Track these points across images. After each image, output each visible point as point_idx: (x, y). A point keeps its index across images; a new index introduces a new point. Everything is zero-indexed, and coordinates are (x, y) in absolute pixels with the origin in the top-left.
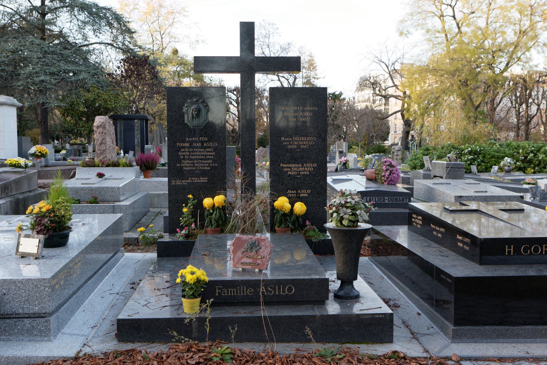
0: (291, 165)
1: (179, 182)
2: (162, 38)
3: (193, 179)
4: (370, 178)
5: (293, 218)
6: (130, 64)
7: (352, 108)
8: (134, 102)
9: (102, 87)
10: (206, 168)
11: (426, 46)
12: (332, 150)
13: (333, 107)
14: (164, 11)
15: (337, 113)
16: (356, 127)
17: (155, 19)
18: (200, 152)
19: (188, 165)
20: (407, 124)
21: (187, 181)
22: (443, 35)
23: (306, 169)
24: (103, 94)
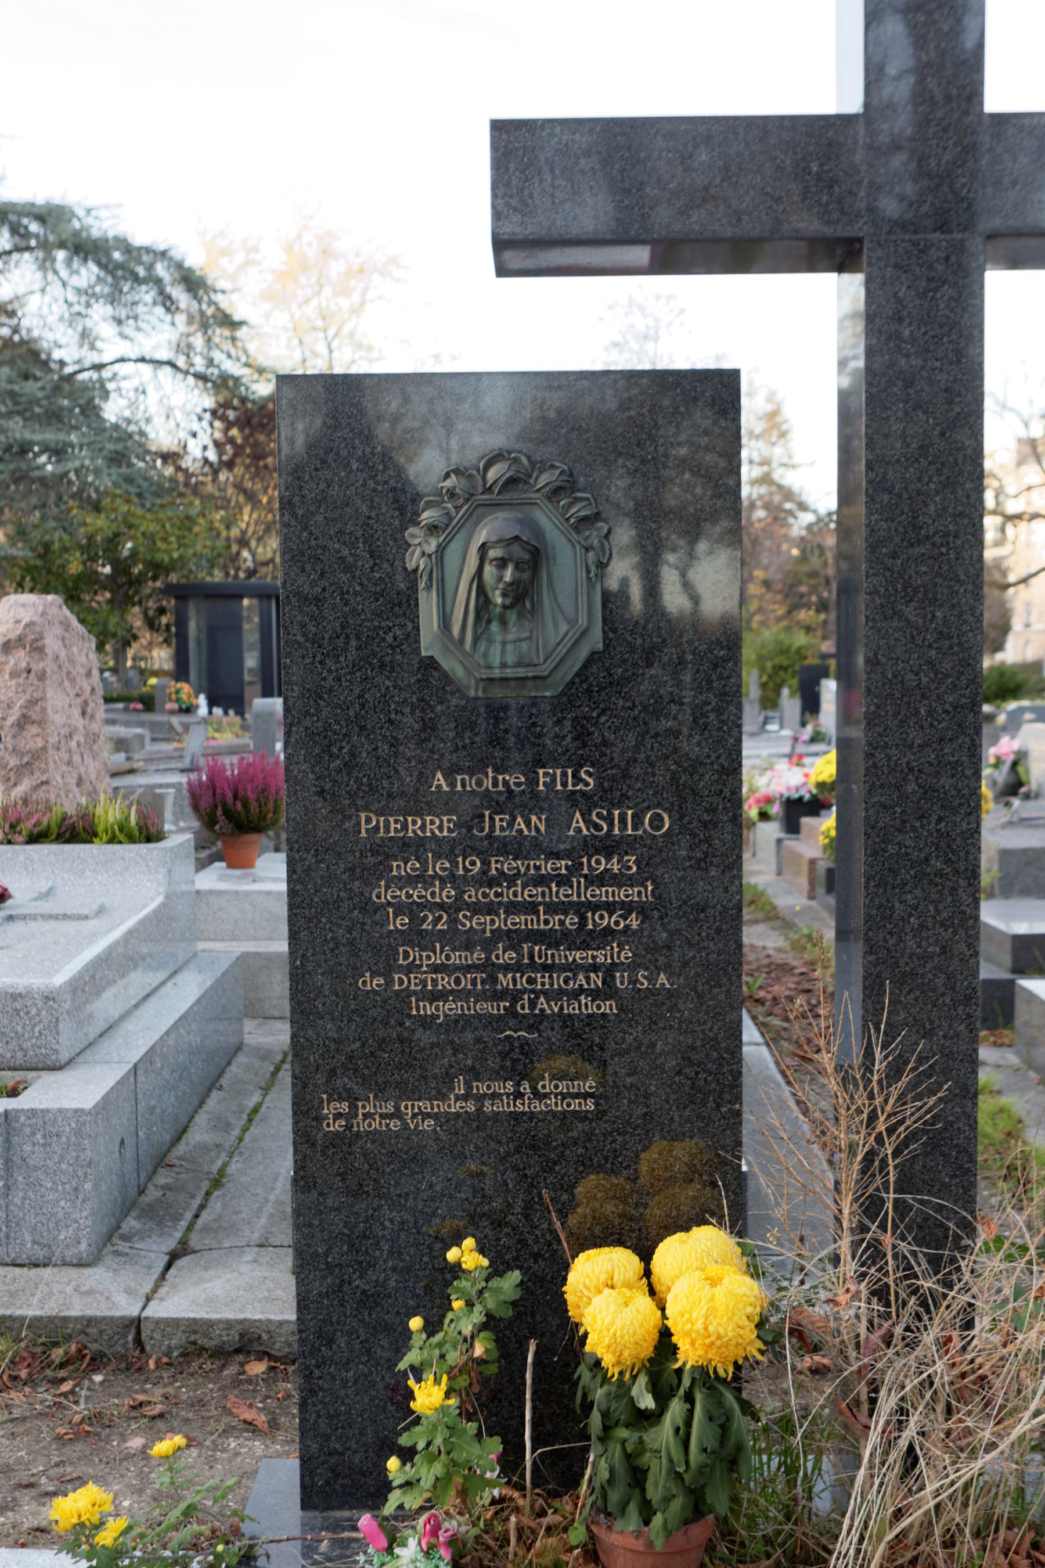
1: (374, 1115)
3: (481, 1088)
6: (229, 425)
8: (243, 542)
9: (140, 495)
10: (587, 1006)
14: (336, 268)
17: (309, 292)
18: (541, 880)
19: (445, 982)
21: (439, 1107)
24: (143, 518)
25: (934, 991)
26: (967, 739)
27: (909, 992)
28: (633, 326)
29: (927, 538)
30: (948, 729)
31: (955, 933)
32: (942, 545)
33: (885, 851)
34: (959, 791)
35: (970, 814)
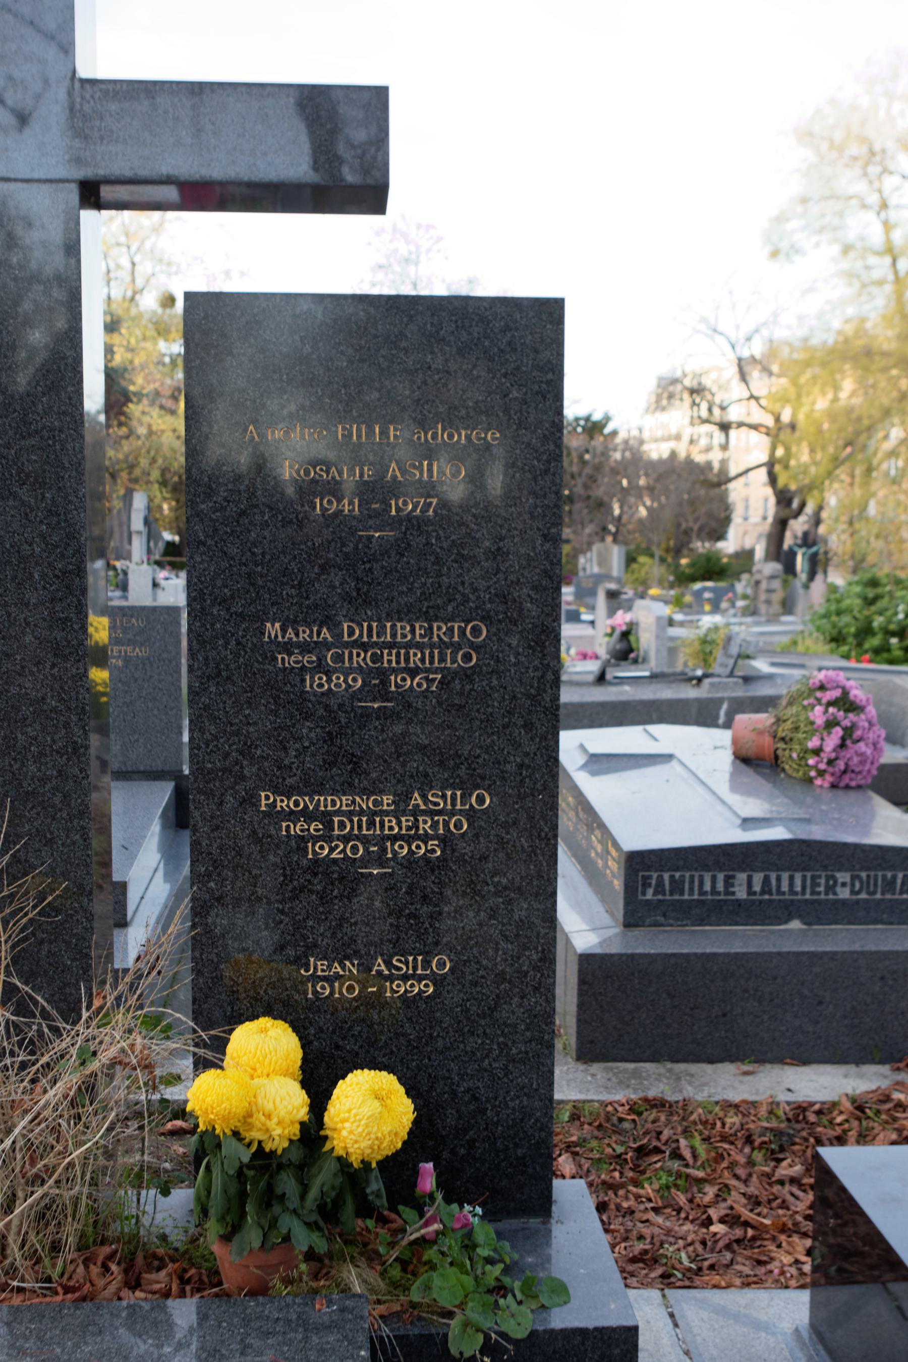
0: (325, 802)
2: (133, 264)
4: (751, 752)
5: (323, 1178)
7: (635, 460)
11: (840, 290)
12: (584, 569)
13: (587, 451)
15: (598, 468)
16: (644, 505)
20: (787, 503)
22: (888, 260)
23: (425, 825)
25: (52, 807)
26: (75, 599)
27: (32, 809)
28: (396, 251)
29: (36, 432)
30: (58, 590)
31: (69, 759)
32: (49, 438)
33: (7, 691)
34: (69, 642)
35: (79, 661)
